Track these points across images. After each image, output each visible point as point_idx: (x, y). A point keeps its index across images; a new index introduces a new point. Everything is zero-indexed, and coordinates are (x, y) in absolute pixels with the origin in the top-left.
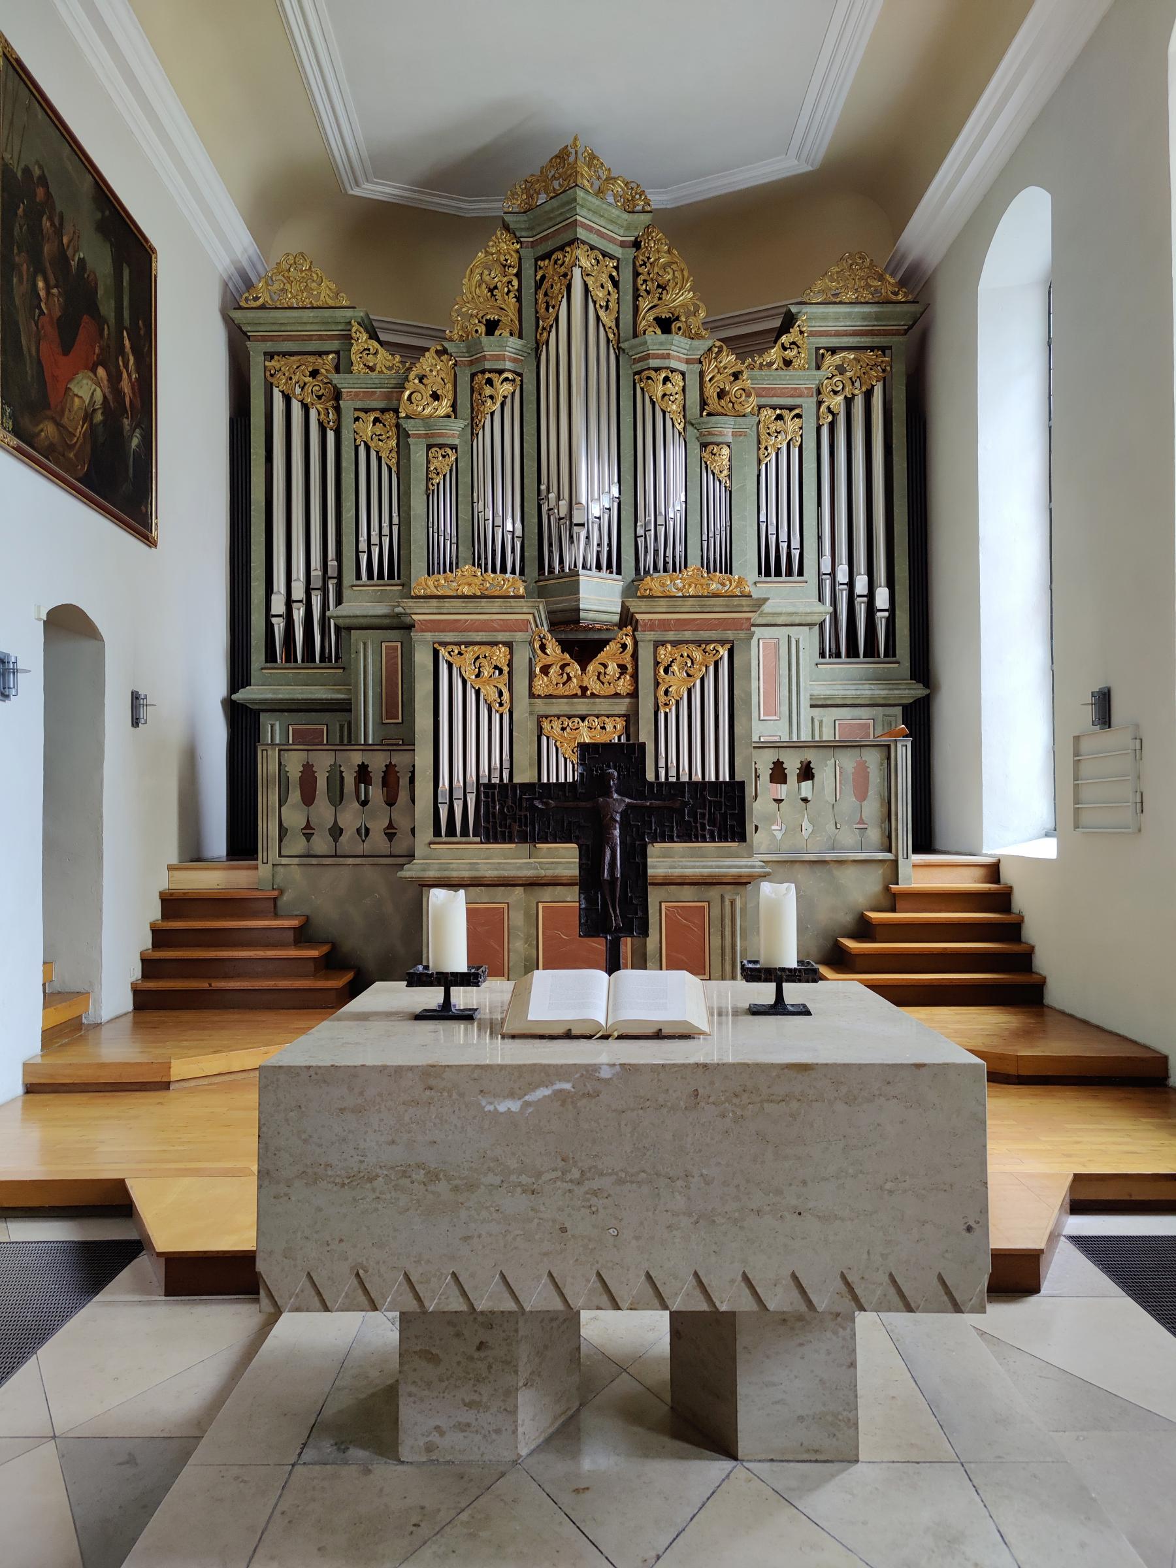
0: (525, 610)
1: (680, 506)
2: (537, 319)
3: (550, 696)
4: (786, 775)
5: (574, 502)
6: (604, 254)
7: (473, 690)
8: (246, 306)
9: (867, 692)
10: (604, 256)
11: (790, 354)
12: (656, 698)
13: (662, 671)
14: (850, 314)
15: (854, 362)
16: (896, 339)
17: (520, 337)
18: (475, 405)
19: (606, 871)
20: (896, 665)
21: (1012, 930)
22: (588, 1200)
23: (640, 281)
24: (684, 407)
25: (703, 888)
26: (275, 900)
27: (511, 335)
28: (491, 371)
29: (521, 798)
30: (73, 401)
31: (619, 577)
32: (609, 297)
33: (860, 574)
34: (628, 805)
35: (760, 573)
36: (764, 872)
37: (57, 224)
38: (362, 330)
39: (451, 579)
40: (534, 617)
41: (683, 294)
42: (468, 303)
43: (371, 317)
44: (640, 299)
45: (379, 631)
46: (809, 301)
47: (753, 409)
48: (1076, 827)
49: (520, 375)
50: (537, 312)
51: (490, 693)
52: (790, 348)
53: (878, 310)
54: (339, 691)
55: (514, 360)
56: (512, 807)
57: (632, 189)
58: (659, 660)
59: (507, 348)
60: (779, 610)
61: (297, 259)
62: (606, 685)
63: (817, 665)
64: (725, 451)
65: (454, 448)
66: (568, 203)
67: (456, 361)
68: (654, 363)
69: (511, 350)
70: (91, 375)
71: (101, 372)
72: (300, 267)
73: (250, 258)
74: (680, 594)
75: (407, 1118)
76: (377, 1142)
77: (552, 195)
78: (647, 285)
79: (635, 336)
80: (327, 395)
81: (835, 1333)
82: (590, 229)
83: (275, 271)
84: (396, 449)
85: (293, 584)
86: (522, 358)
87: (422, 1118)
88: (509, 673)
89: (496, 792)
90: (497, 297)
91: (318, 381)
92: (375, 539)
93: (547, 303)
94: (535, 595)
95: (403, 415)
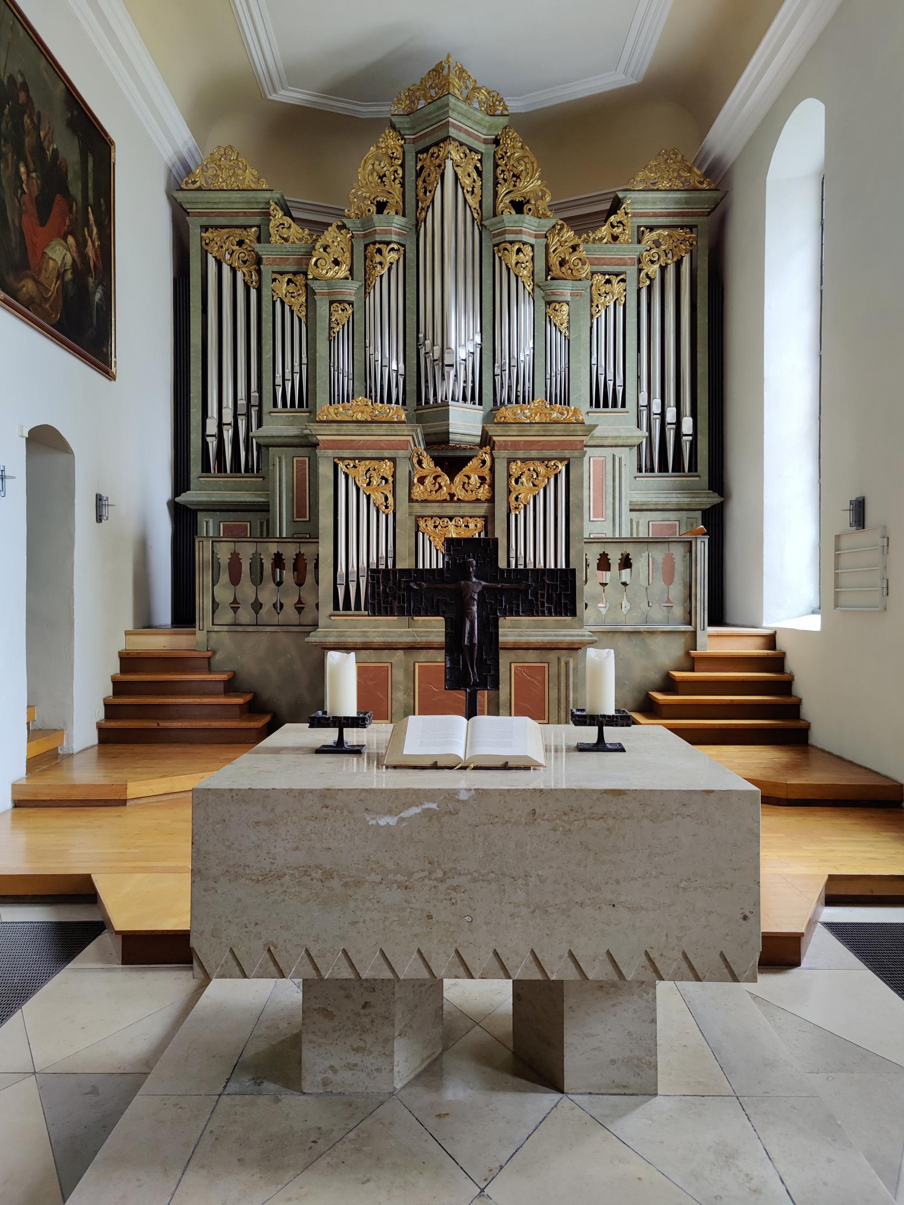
0: (406, 433)
1: (529, 352)
2: (417, 201)
3: (426, 501)
4: (610, 564)
5: (445, 347)
6: (471, 150)
7: (365, 496)
8: (185, 188)
10: (470, 151)
11: (617, 231)
12: (509, 503)
13: (513, 482)
15: (668, 238)
16: (701, 219)
17: (404, 215)
18: (368, 269)
19: (466, 638)
20: (698, 479)
21: (785, 686)
22: (449, 894)
23: (499, 171)
24: (533, 272)
25: (544, 652)
26: (209, 658)
28: (380, 242)
29: (400, 580)
30: (48, 262)
31: (481, 407)
32: (474, 184)
33: (670, 406)
34: (484, 587)
35: (591, 405)
36: (592, 640)
37: (36, 121)
38: (278, 208)
40: (413, 438)
41: (533, 182)
43: (286, 198)
44: (499, 185)
45: (291, 448)
47: (587, 274)
48: (836, 606)
49: (403, 246)
50: (417, 196)
52: (618, 226)
54: (259, 496)
55: (399, 234)
57: (493, 96)
58: (511, 473)
59: (394, 224)
60: (606, 434)
61: (227, 151)
62: (469, 492)
64: (565, 308)
65: (351, 303)
67: (353, 234)
68: (509, 237)
69: (396, 225)
70: (63, 242)
71: (71, 240)
73: (189, 150)
75: (308, 830)
76: (285, 848)
77: (430, 101)
78: (504, 175)
79: (495, 215)
81: (641, 997)
82: (459, 129)
83: (209, 160)
84: (305, 304)
87: (320, 829)
88: (393, 482)
90: (385, 183)
92: (288, 376)
93: (425, 188)
94: (415, 421)
95: (310, 277)
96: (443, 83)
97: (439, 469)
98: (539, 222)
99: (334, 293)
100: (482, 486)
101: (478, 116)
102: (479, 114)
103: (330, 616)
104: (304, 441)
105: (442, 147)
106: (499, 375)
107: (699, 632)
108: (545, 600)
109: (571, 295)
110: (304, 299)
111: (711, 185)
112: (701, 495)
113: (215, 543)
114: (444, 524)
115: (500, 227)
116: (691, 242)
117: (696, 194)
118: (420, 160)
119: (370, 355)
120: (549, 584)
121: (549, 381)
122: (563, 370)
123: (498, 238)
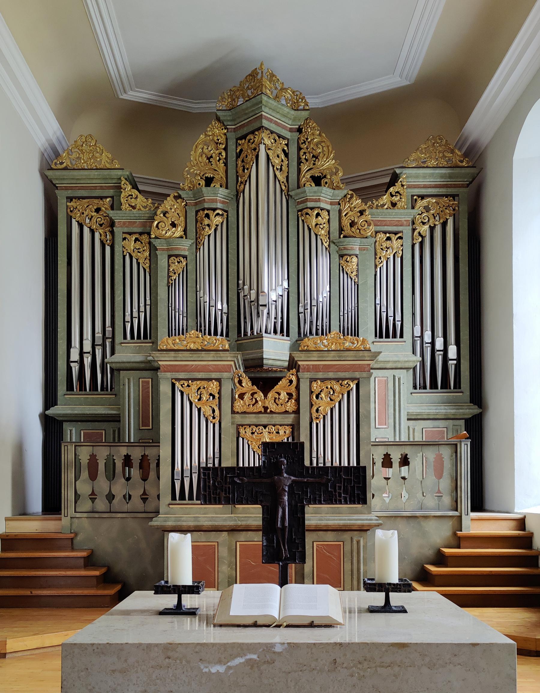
0: (229, 359)
1: (326, 294)
2: (237, 177)
3: (245, 413)
4: (392, 462)
6: (280, 136)
7: (196, 409)
8: (55, 168)
9: (443, 411)
10: (279, 137)
11: (395, 199)
12: (311, 414)
15: (436, 204)
16: (462, 190)
18: (198, 230)
20: (461, 394)
25: (340, 533)
26: (72, 539)
27: (221, 186)
28: (208, 209)
29: (226, 477)
33: (439, 337)
34: (293, 481)
35: (376, 336)
36: (378, 523)
38: (128, 183)
39: (183, 339)
40: (235, 363)
41: (328, 161)
42: (194, 166)
43: (134, 175)
44: (302, 164)
45: (138, 371)
46: (407, 166)
47: (372, 233)
49: (226, 211)
50: (237, 172)
51: (207, 410)
52: (395, 195)
53: (450, 171)
54: (112, 409)
55: (223, 202)
56: (220, 481)
57: (297, 95)
58: (313, 390)
59: (219, 195)
60: (388, 359)
61: (87, 139)
63: (411, 393)
64: (355, 260)
65: (185, 257)
66: (257, 104)
67: (186, 203)
68: (310, 204)
69: (221, 196)
74: (326, 349)
75: (154, 677)
77: (247, 99)
78: (306, 156)
79: (299, 187)
83: (74, 146)
84: (149, 258)
85: (84, 342)
88: (219, 398)
90: (212, 163)
91: (100, 215)
92: (135, 314)
93: (244, 166)
94: (236, 349)
95: (153, 236)
96: (257, 85)
97: (256, 387)
98: (333, 193)
99: (172, 249)
103: (169, 504)
105: (257, 135)
106: (302, 313)
108: (342, 491)
110: (148, 254)
112: (464, 407)
113: (77, 447)
114: (259, 431)
115: (303, 196)
116: (454, 208)
117: (457, 171)
119: (200, 297)
120: (344, 479)
121: (342, 318)
122: (353, 308)
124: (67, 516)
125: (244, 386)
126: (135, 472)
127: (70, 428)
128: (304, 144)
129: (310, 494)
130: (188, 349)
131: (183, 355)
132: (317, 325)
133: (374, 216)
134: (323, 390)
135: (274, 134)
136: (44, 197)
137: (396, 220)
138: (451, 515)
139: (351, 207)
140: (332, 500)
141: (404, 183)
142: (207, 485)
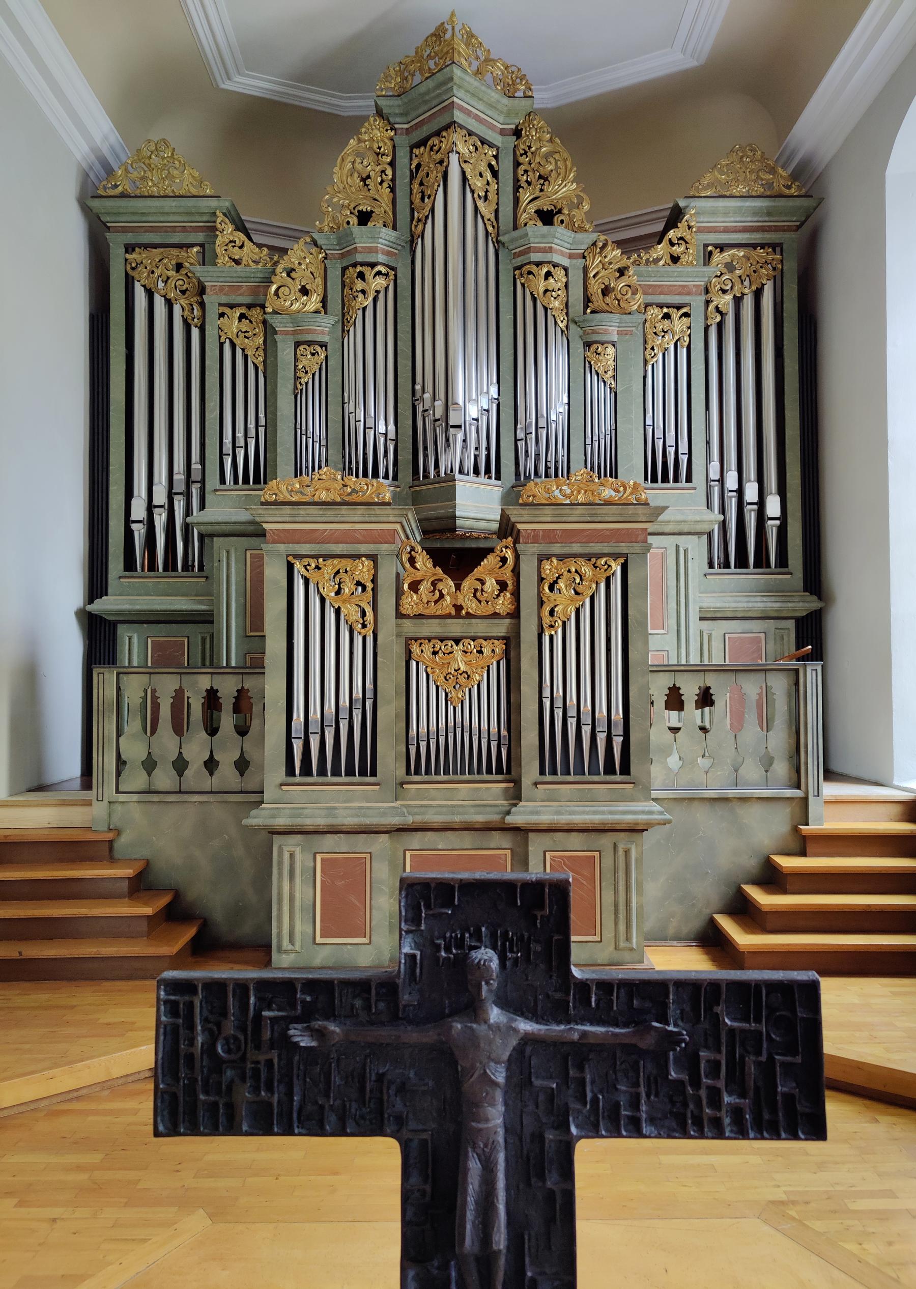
0: (391, 519)
1: (562, 409)
3: (420, 616)
4: (683, 702)
5: (450, 402)
7: (332, 609)
8: (104, 194)
9: (760, 605)
10: (483, 143)
11: (677, 250)
12: (540, 619)
13: (546, 589)
14: (740, 208)
15: (744, 259)
18: (346, 300)
19: (469, 1227)
20: (789, 576)
25: (593, 835)
26: (111, 842)
27: (385, 226)
28: (363, 264)
29: (258, 1017)
32: (487, 187)
33: (750, 481)
34: (527, 1040)
35: (646, 479)
36: (664, 820)
39: (308, 483)
40: (403, 527)
41: (566, 186)
42: (339, 192)
43: (243, 218)
44: (521, 190)
45: (243, 538)
46: (697, 195)
47: (639, 306)
50: (412, 203)
51: (351, 612)
52: (678, 244)
54: (200, 602)
56: (236, 1038)
57: (513, 72)
58: (543, 576)
59: (380, 240)
61: (159, 146)
63: (705, 575)
64: (610, 350)
65: (324, 345)
66: (444, 83)
67: (326, 254)
68: (535, 257)
69: (384, 242)
72: (162, 154)
73: (112, 147)
74: (568, 502)
78: (528, 176)
79: (515, 228)
80: (192, 290)
82: (468, 113)
83: (136, 158)
84: (263, 347)
85: (155, 488)
86: (397, 251)
88: (373, 589)
89: (197, 1004)
90: (370, 187)
91: (181, 275)
92: (241, 442)
93: (423, 192)
94: (410, 501)
95: (269, 310)
96: (445, 50)
97: (440, 570)
98: (574, 238)
100: (502, 594)
101: (492, 97)
102: (493, 94)
103: (281, 785)
104: (251, 528)
105: (445, 137)
106: (522, 439)
107: (811, 799)
108: (721, 1084)
109: (618, 334)
110: (261, 341)
111: (801, 190)
112: (794, 599)
113: (121, 676)
114: (447, 649)
115: (523, 243)
116: (774, 266)
117: (781, 202)
118: (416, 156)
119: (349, 413)
120: (731, 1031)
121: (589, 448)
123: (519, 259)
124: (102, 800)
125: (419, 567)
126: (227, 721)
127: (129, 634)
128: (525, 156)
129: (592, 1091)
130: (316, 500)
131: (308, 512)
132: (546, 461)
133: (642, 279)
134: (562, 575)
135: (473, 137)
136: (87, 248)
137: (680, 285)
138: (788, 796)
139: (604, 262)
140: (684, 1116)
141: (692, 224)
142: (182, 1054)
